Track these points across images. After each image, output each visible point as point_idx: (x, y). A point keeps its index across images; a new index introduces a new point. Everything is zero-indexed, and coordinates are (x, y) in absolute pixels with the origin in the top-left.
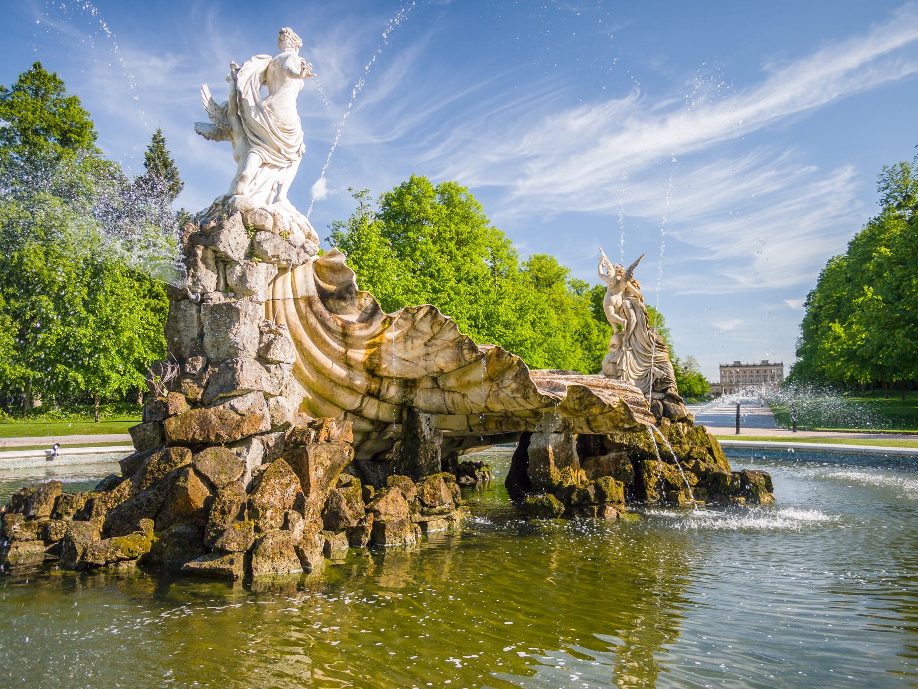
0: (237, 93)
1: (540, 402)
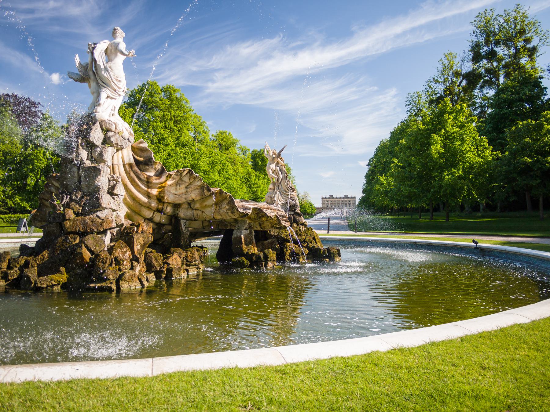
0: (94, 60)
1: (239, 215)
